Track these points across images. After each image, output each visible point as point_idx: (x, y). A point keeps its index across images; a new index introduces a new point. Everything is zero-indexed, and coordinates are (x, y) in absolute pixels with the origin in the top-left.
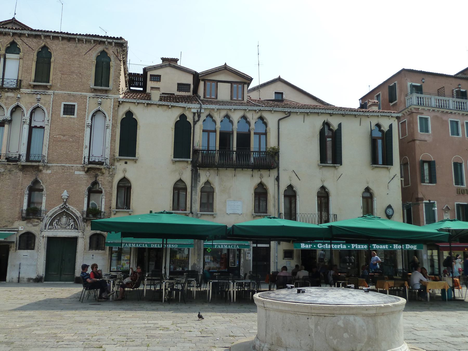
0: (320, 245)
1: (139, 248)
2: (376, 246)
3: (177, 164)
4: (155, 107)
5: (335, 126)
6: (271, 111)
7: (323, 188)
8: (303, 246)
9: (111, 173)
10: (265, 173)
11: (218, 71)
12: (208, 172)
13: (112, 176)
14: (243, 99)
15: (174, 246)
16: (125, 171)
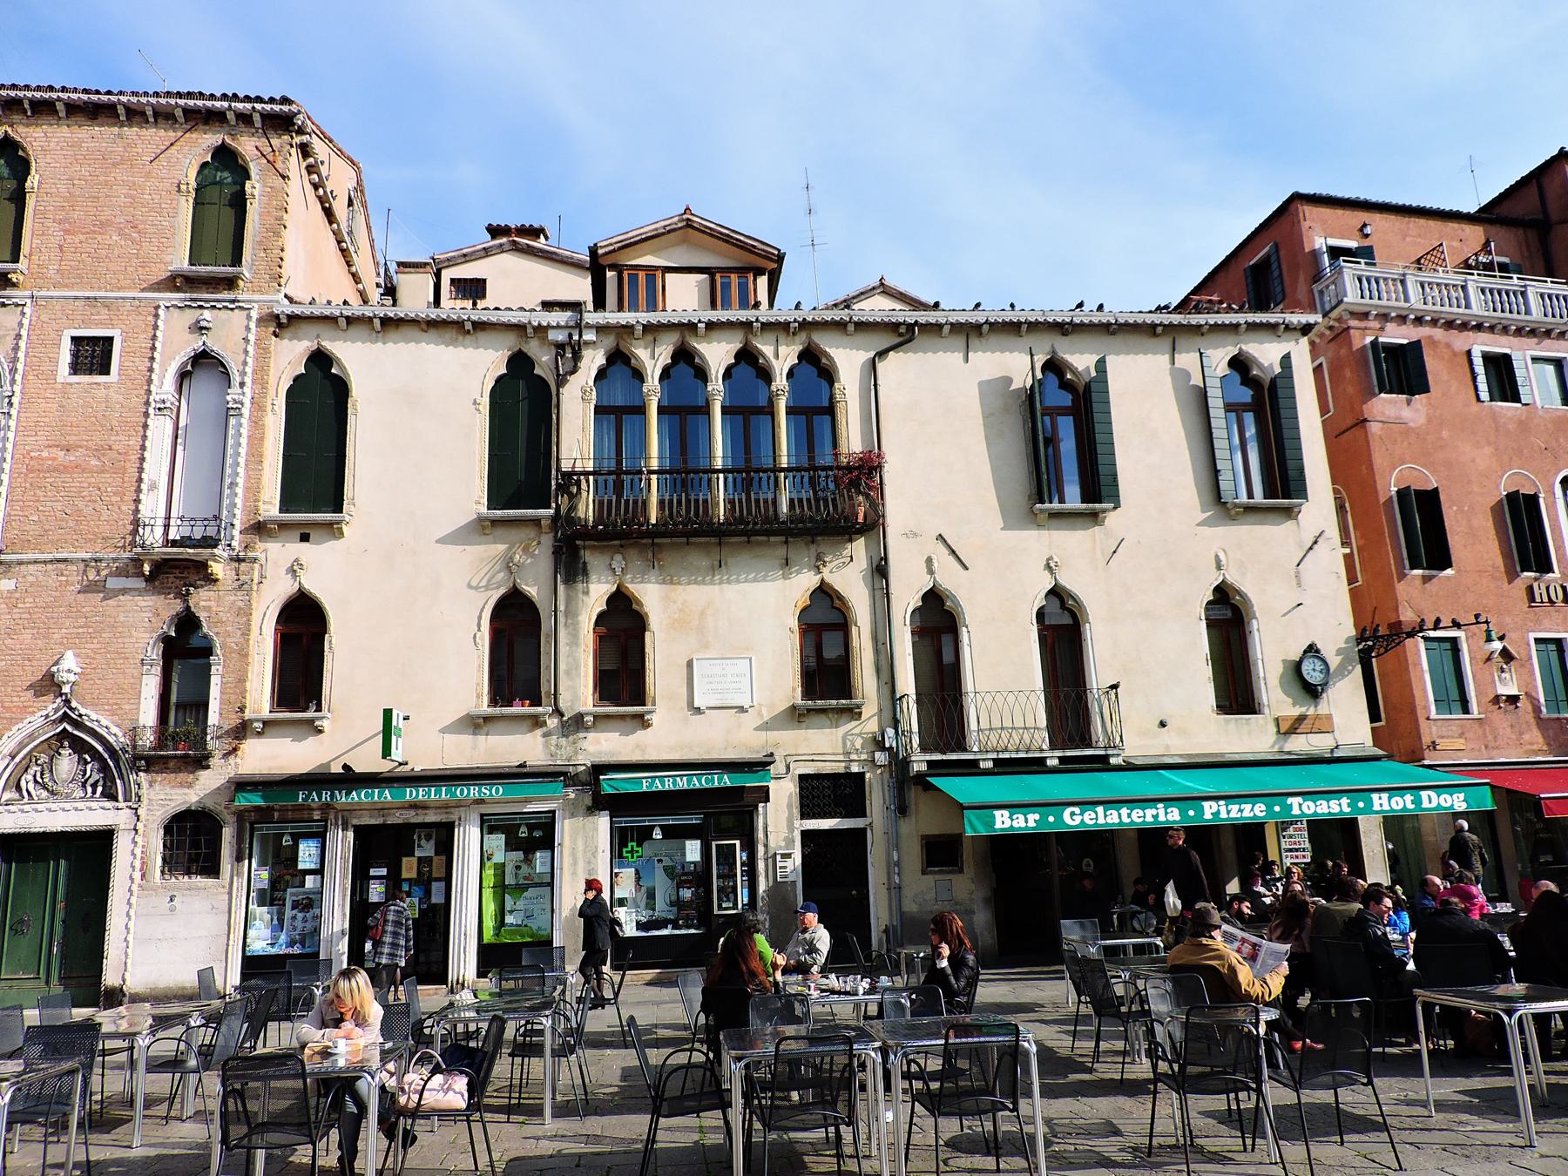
0: (1072, 814)
8: (1003, 819)
15: (490, 790)
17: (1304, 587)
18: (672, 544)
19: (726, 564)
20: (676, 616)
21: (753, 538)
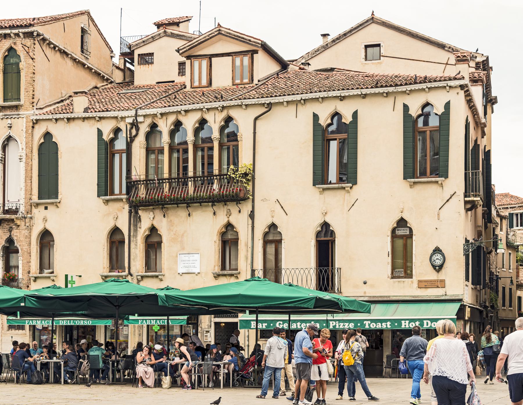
0: (280, 324)
1: (66, 326)
2: (369, 325)
3: (110, 204)
4: (80, 122)
5: (347, 119)
6: (240, 106)
7: (325, 226)
9: (27, 224)
10: (233, 208)
11: (208, 39)
12: (151, 213)
13: (30, 228)
14: (253, 81)
16: (45, 220)
17: (441, 220)
18: (173, 207)
19: (192, 215)
20: (173, 237)
21: (202, 204)
